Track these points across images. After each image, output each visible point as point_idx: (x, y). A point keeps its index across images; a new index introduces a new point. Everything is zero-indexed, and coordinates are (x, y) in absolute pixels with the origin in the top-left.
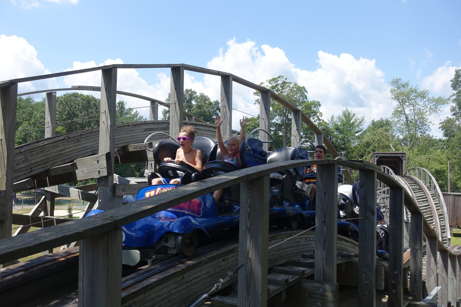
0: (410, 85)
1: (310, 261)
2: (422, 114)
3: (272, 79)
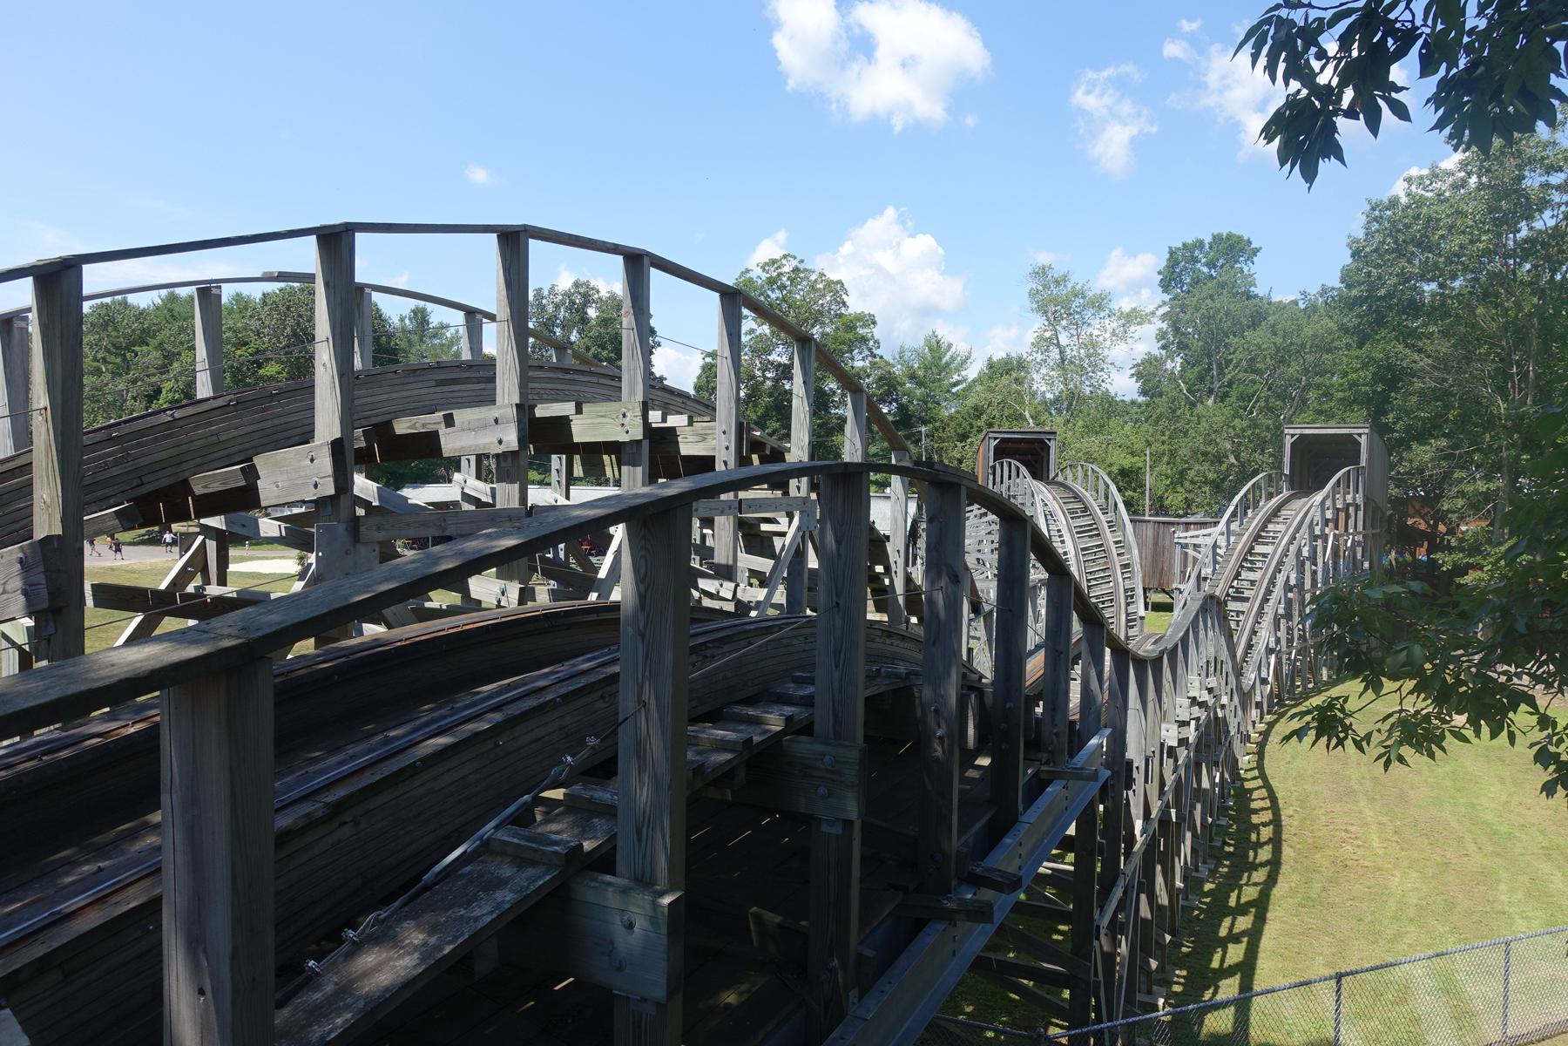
1: (809, 690)
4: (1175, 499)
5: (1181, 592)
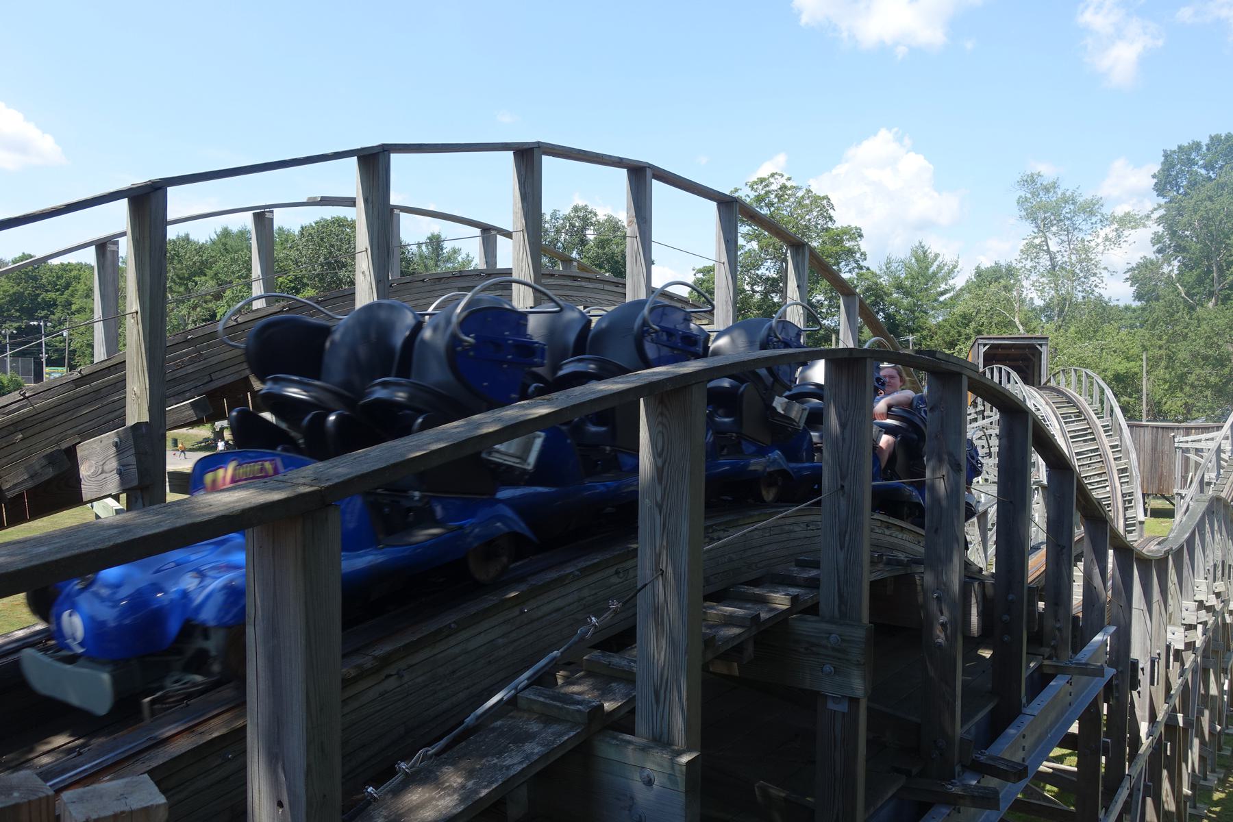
0: (1061, 187)
1: (813, 573)
2: (1086, 251)
3: (758, 179)
4: (1174, 404)
5: (1182, 498)
